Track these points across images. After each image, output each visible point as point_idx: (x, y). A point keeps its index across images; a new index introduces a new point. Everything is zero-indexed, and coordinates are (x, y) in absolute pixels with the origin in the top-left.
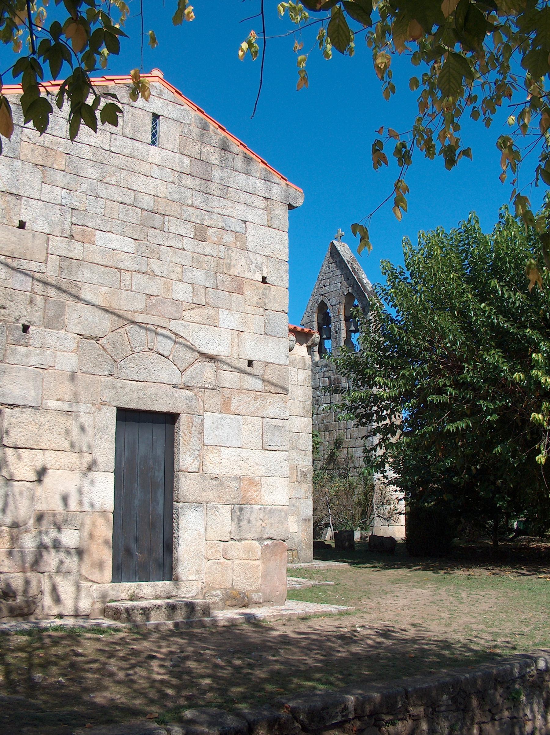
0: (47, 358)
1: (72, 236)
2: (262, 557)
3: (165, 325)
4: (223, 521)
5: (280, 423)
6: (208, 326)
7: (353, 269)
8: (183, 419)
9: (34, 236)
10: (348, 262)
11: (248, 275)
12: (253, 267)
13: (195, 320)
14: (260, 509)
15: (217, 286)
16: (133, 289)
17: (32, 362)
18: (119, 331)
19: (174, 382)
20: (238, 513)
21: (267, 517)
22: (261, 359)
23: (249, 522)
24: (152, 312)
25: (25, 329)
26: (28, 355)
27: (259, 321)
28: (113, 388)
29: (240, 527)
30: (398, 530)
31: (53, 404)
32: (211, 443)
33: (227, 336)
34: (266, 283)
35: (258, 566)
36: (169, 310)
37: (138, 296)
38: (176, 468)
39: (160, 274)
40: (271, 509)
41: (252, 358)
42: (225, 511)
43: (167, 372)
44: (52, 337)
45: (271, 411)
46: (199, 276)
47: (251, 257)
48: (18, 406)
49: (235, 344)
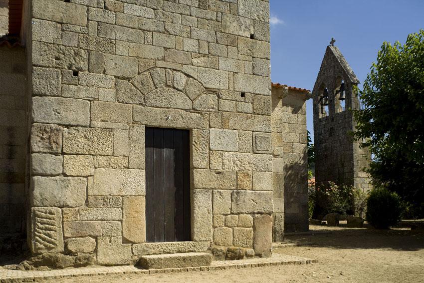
0: (92, 92)
1: (106, 8)
2: (305, 130)
3: (179, 69)
4: (224, 202)
5: (265, 135)
6: (211, 69)
7: (341, 61)
8: (195, 132)
9: (76, 7)
10: (338, 58)
11: (241, 33)
12: (243, 27)
13: (201, 65)
14: (252, 193)
15: (217, 41)
16: (154, 44)
17: (81, 96)
18: (145, 73)
19: (187, 107)
20: (236, 196)
21: (257, 198)
22: (250, 91)
23: (244, 201)
24: (168, 60)
25: (76, 74)
26: (79, 90)
27: (249, 65)
28: (143, 112)
29: (238, 205)
30: (344, 97)
31: (99, 124)
32: (215, 148)
33: (225, 75)
34: (253, 39)
35: (250, 232)
36: (182, 58)
37: (158, 48)
38: (191, 167)
39: (173, 33)
40: (260, 193)
41: (244, 91)
42: (227, 194)
43: (180, 101)
44: (95, 78)
45: (258, 127)
46: (202, 34)
47: (242, 20)
48: (72, 126)
49: (232, 82)
